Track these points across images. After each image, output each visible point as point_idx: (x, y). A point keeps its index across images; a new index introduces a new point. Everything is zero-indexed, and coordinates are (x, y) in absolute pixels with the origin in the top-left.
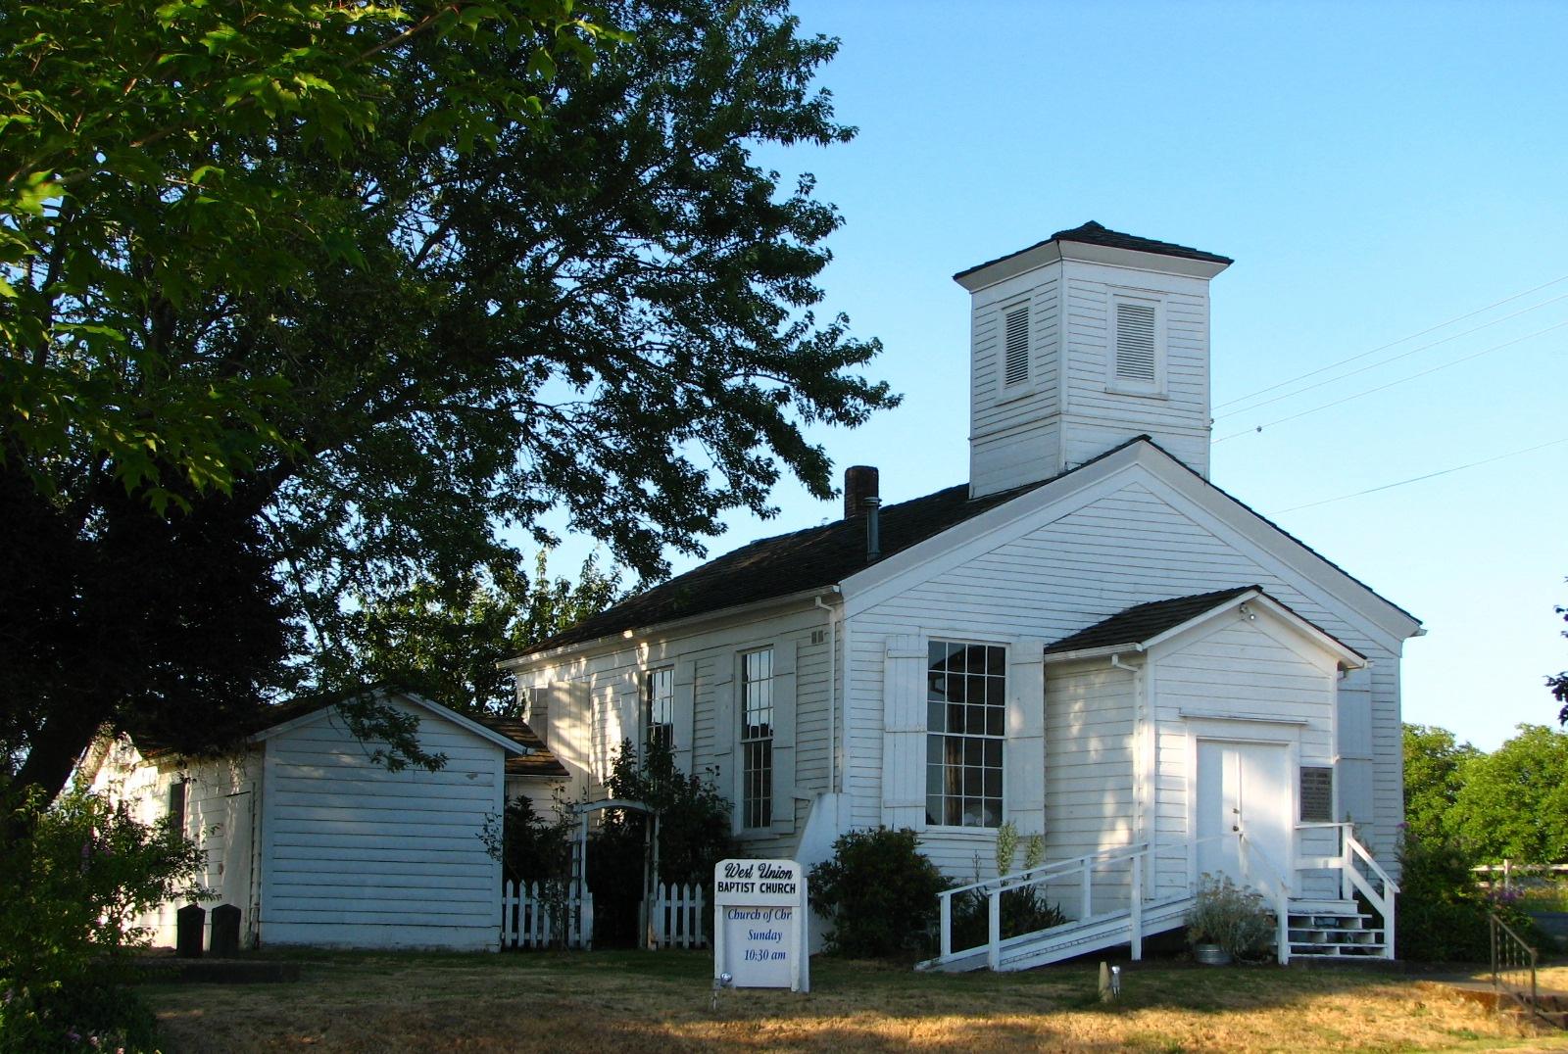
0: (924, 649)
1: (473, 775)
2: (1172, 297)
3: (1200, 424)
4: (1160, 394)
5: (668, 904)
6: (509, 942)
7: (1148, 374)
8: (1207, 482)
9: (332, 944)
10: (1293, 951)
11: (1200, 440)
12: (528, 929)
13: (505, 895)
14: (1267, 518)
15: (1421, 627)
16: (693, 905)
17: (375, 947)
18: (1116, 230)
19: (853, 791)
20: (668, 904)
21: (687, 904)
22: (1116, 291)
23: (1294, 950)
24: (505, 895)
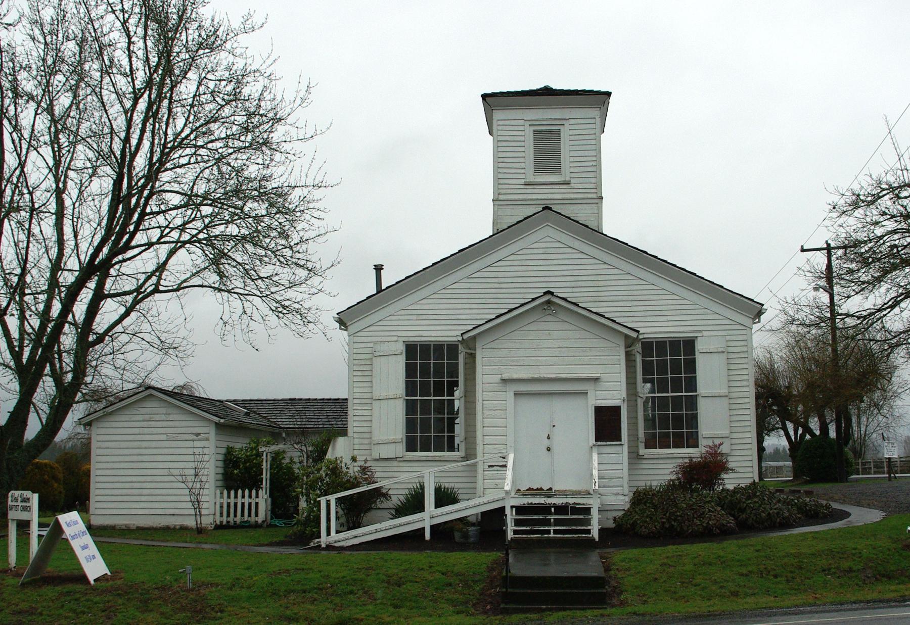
0: (401, 348)
1: (198, 435)
2: (572, 121)
3: (594, 196)
4: (564, 181)
5: (222, 500)
6: (218, 523)
7: (557, 169)
8: (602, 234)
9: (126, 525)
10: (514, 534)
11: (596, 205)
12: (235, 516)
13: (215, 497)
14: (639, 248)
15: (764, 307)
16: (229, 501)
17: (155, 526)
18: (558, 88)
19: (356, 436)
20: (222, 500)
21: (240, 501)
22: (531, 123)
23: (516, 532)
24: (215, 497)
